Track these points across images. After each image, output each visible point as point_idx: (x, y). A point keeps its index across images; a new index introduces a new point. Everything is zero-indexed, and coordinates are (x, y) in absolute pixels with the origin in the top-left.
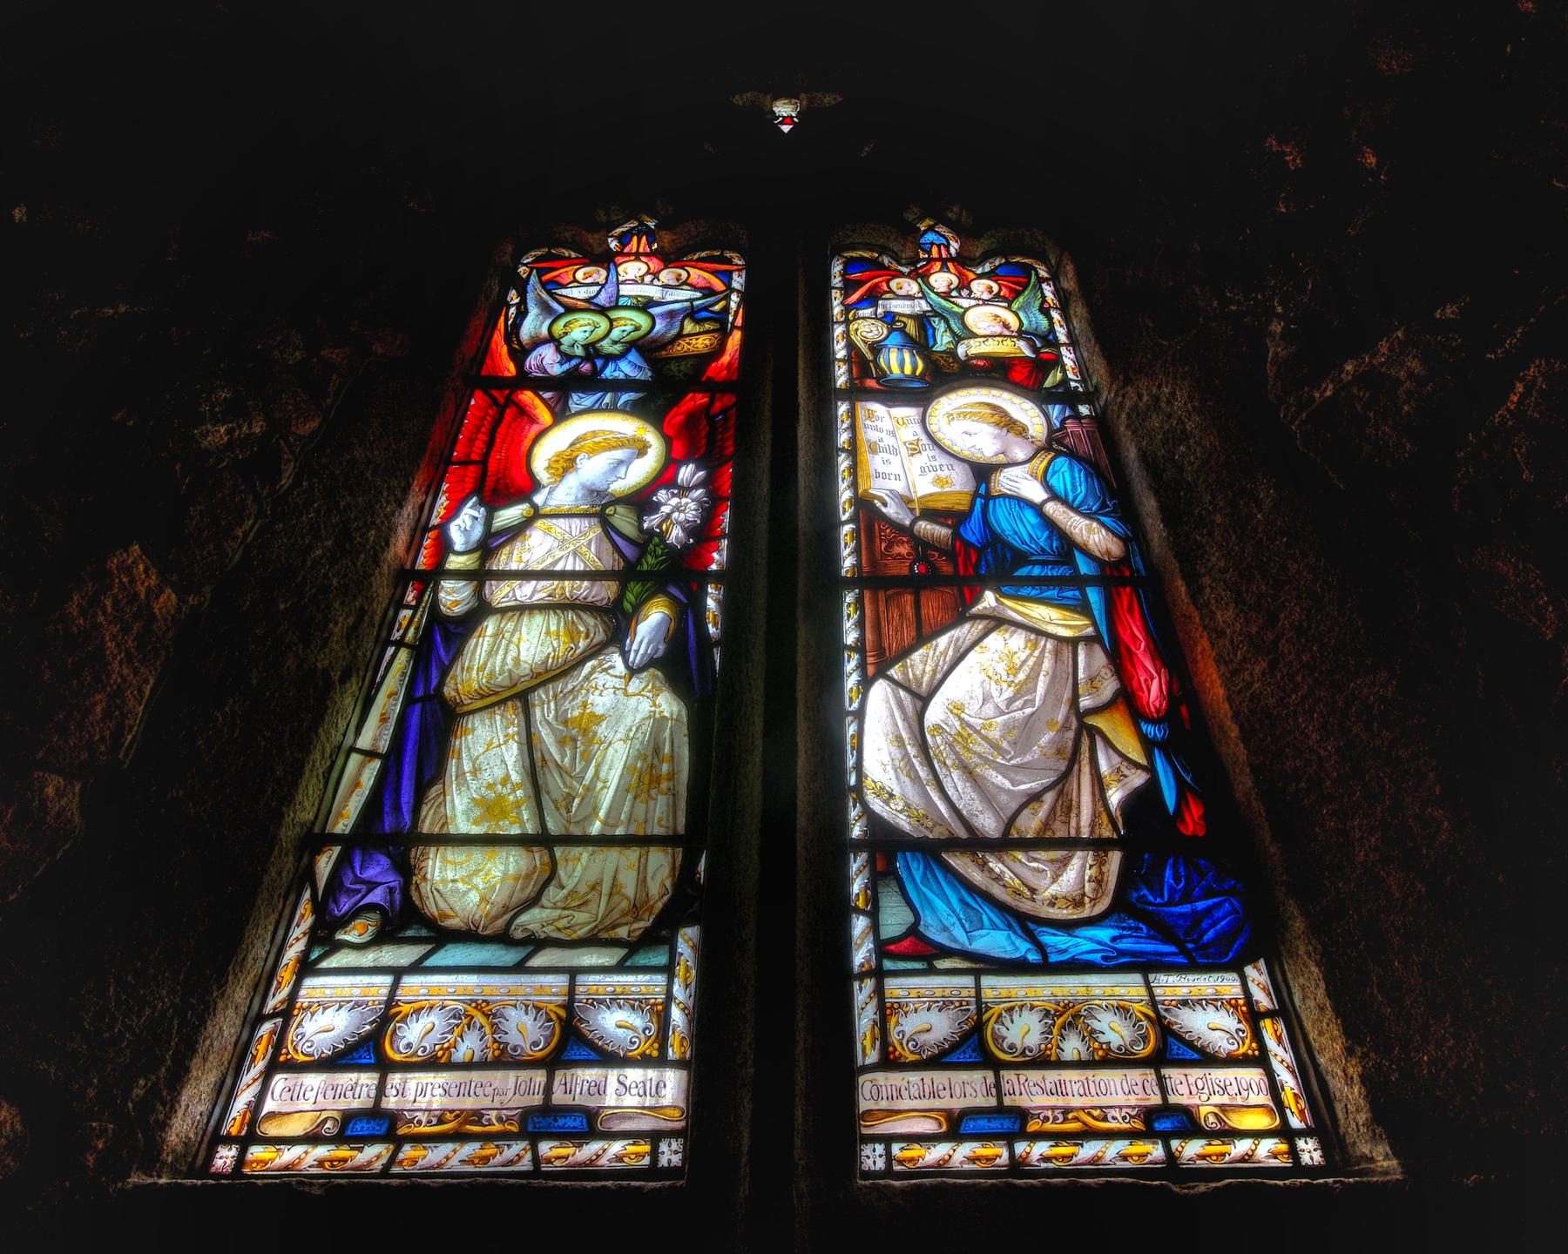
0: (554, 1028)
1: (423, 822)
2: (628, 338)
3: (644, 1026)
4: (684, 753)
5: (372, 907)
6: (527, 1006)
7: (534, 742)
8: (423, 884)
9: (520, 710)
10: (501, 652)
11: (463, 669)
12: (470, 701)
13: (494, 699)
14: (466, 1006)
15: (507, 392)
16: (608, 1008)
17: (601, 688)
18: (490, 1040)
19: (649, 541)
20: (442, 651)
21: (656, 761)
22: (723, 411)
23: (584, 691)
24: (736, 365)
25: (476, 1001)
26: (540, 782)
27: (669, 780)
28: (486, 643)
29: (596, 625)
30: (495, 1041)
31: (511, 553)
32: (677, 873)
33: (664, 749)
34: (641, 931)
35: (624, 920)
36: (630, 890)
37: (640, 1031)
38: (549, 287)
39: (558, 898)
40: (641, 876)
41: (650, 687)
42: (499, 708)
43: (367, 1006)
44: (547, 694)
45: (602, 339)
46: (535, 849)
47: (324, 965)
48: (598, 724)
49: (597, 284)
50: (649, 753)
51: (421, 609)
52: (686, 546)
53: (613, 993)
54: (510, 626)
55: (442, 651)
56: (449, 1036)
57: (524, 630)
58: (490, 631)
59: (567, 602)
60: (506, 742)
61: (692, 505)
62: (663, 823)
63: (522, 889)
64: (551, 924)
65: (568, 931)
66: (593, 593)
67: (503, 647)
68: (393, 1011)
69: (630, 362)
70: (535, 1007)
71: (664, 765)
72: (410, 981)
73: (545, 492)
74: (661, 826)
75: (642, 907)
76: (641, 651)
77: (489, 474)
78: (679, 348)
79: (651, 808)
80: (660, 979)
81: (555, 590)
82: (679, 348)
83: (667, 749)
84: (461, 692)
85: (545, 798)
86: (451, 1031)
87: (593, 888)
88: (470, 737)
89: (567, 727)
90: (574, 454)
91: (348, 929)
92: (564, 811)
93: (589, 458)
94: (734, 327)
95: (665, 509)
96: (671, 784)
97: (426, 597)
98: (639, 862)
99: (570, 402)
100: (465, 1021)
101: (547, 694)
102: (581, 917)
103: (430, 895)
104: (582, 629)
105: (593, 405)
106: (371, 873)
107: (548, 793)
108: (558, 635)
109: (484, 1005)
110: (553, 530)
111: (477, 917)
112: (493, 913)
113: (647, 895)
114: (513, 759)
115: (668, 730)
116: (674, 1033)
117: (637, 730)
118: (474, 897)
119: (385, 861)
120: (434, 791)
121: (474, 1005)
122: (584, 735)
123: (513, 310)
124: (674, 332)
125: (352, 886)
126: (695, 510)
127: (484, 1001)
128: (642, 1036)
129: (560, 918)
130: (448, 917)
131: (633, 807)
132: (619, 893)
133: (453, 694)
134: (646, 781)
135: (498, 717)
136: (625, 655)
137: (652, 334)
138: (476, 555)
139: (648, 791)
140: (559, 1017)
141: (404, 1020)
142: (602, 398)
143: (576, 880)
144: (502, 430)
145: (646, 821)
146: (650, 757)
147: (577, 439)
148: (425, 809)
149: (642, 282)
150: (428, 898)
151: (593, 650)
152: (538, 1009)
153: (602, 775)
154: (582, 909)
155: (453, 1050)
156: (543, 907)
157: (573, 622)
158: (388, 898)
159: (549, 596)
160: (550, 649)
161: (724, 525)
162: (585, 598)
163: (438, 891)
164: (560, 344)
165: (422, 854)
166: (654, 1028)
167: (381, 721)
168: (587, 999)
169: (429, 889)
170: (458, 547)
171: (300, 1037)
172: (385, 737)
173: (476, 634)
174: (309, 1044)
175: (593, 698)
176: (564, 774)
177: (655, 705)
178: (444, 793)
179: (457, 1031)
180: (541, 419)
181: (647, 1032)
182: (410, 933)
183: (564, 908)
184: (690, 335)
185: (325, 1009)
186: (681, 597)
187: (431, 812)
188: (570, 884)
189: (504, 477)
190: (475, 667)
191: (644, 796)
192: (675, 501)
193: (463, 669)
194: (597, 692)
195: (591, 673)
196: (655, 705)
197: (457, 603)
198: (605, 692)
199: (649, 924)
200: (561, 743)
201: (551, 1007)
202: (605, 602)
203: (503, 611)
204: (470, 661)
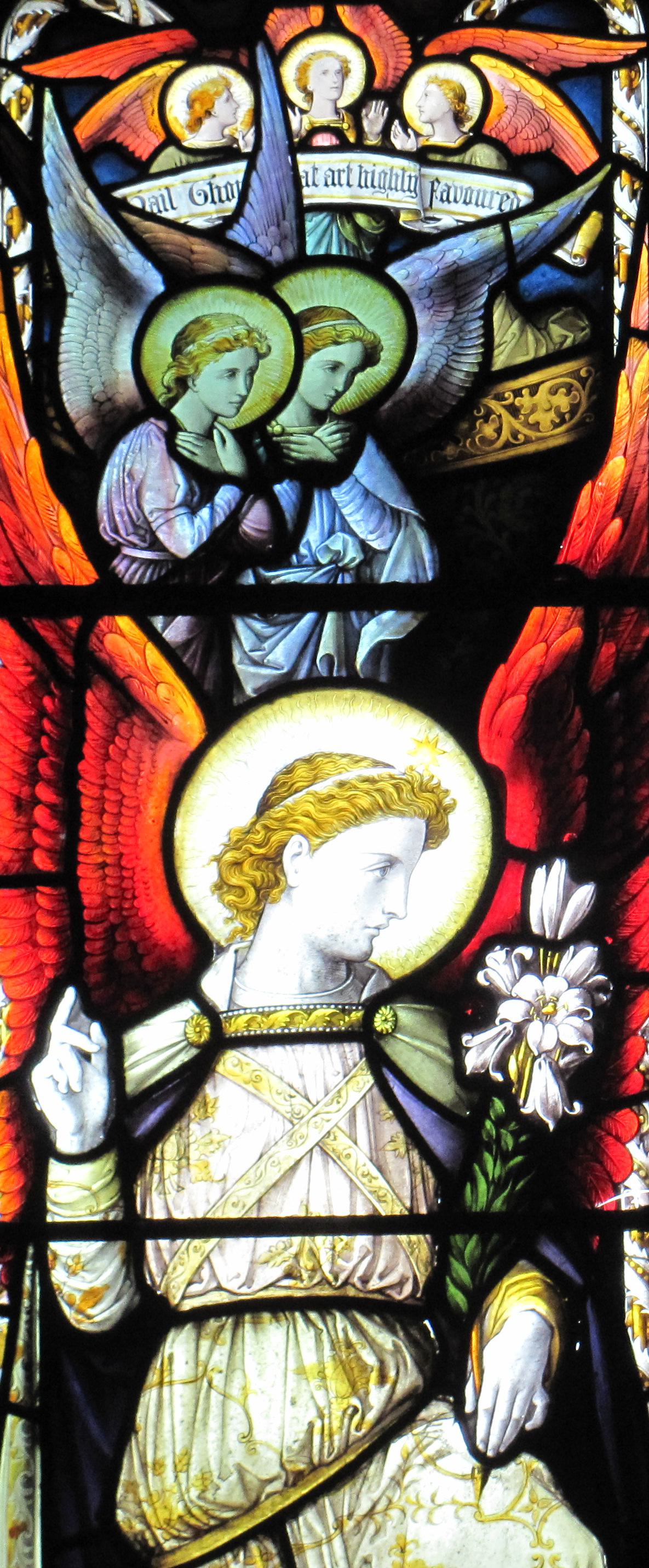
2: (350, 399)
10: (214, 1423)
13: (223, 1538)
17: (430, 1505)
19: (482, 1111)
20: (94, 1428)
23: (394, 1513)
28: (177, 1402)
29: (397, 1349)
31: (183, 1155)
38: (105, 175)
41: (525, 1500)
44: (322, 1516)
49: (226, 154)
52: (564, 1121)
54: (220, 1356)
55: (94, 1428)
57: (250, 1364)
61: (573, 1000)
66: (380, 1268)
67: (215, 1410)
81: (296, 1256)
84: (152, 1521)
90: (276, 838)
93: (313, 850)
95: (509, 1012)
101: (322, 1516)
104: (370, 1359)
108: (322, 1376)
110: (263, 1085)
124: (469, 363)
133: (139, 1527)
136: (466, 1421)
137: (411, 377)
149: (315, 1005)
157: (349, 1345)
162: (365, 1280)
170: (66, 1142)
173: (153, 1377)
175: (415, 1529)
180: (176, 721)
186: (568, 1269)
189: (124, 923)
190: (169, 1462)
193: (144, 1465)
194: (422, 1515)
195: (403, 1471)
196: (539, 1541)
198: (438, 1515)
202: (408, 1289)
203: (200, 1316)
204: (156, 1448)
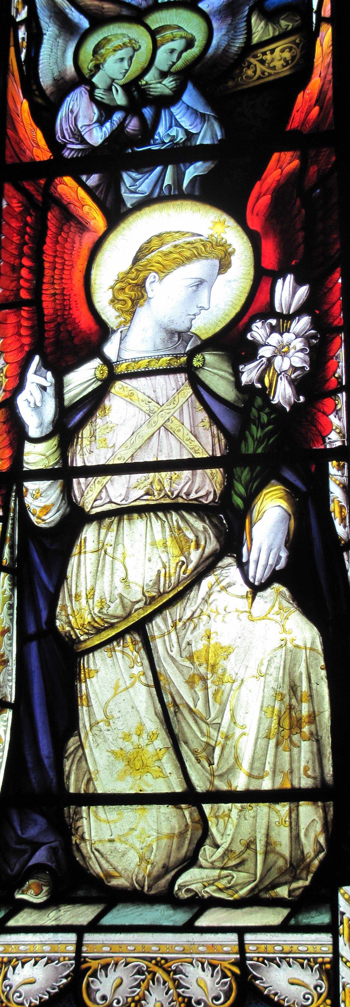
0: (231, 984)
1: (68, 778)
3: (315, 983)
4: (324, 690)
5: (40, 868)
6: (203, 964)
7: (162, 684)
8: (83, 845)
9: (140, 645)
10: (107, 572)
11: (70, 596)
12: (85, 637)
13: (112, 633)
14: (147, 963)
15: (42, 182)
16: (279, 966)
18: (175, 994)
19: (249, 404)
21: (294, 701)
22: (323, 179)
24: (330, 93)
25: (155, 958)
26: (176, 731)
27: (310, 723)
30: (179, 995)
32: (330, 829)
33: (301, 686)
34: (300, 891)
35: (283, 880)
36: (284, 848)
37: (312, 987)
39: (214, 858)
40: (294, 833)
41: (276, 608)
42: (118, 644)
43: (59, 962)
44: (165, 620)
45: (146, 71)
46: (183, 806)
47: (12, 923)
48: (226, 658)
50: (285, 691)
51: (10, 522)
52: (295, 406)
53: (282, 952)
56: (138, 990)
58: (91, 545)
59: (168, 501)
60: (132, 685)
61: (299, 344)
62: (309, 773)
63: (179, 848)
64: (213, 884)
65: (230, 892)
68: (84, 966)
69: (188, 107)
70: (210, 964)
71: (303, 704)
72: (89, 938)
73: (115, 339)
74: (309, 777)
75: (298, 866)
76: (262, 562)
77: (46, 319)
78: (250, 72)
79: (296, 757)
80: (327, 938)
81: (151, 484)
82: (250, 72)
83: (304, 687)
84: (74, 625)
85: (184, 749)
86: (138, 986)
87: (248, 847)
88: (94, 680)
89: (193, 663)
91: (24, 888)
92: (206, 764)
93: (161, 280)
94: (321, 20)
95: (266, 352)
96: (313, 727)
97: (12, 504)
98: (290, 817)
99: (123, 189)
100: (149, 977)
101: (165, 620)
102: (240, 876)
103: (92, 856)
104: (191, 536)
105: (152, 192)
106: (32, 832)
107: (186, 743)
108: (165, 545)
109: (163, 962)
111: (140, 877)
112: (155, 873)
113: (302, 852)
114: (144, 705)
115: (303, 664)
116: (344, 989)
117: (269, 665)
118: (133, 858)
119: (41, 821)
120: (72, 743)
121: (154, 962)
122: (213, 673)
123: (22, 33)
124: (239, 42)
125: (18, 847)
126: (302, 350)
127: (162, 958)
128: (314, 993)
129: (220, 878)
130: (113, 877)
131: (276, 756)
132: (274, 851)
134: (286, 724)
135: (119, 655)
137: (211, 51)
138: (53, 442)
139: (290, 737)
140: (233, 973)
141: (94, 975)
142: (162, 175)
143: (229, 839)
144: (48, 248)
145: (291, 771)
146: (287, 698)
147: (140, 250)
148: (67, 764)
150: (90, 858)
151: (208, 562)
152: (214, 967)
153: (239, 720)
154: (240, 869)
155: (143, 1002)
156: (201, 867)
157: (179, 529)
158: (53, 858)
159: (147, 494)
160: (160, 566)
161: (339, 371)
163: (98, 850)
164: (93, 87)
165: (76, 813)
166: (325, 985)
167: (111, 301)
168: (258, 958)
169: (89, 848)
170: (33, 432)
171: (8, 988)
172: (10, 684)
173: (76, 550)
174: (18, 994)
176: (200, 722)
177: (285, 631)
178: (81, 746)
179: (143, 985)
181: (318, 989)
182: (81, 893)
183: (223, 868)
184: (262, 44)
185: (23, 964)
186: (298, 483)
187: (74, 767)
188: (224, 843)
189: (64, 322)
191: (286, 743)
192: (275, 338)
193: (70, 596)
194: (220, 618)
195: (209, 595)
196: (285, 631)
197: (46, 509)
199: (307, 883)
200: (191, 683)
201: (226, 964)
202: (211, 497)
203: (100, 517)
